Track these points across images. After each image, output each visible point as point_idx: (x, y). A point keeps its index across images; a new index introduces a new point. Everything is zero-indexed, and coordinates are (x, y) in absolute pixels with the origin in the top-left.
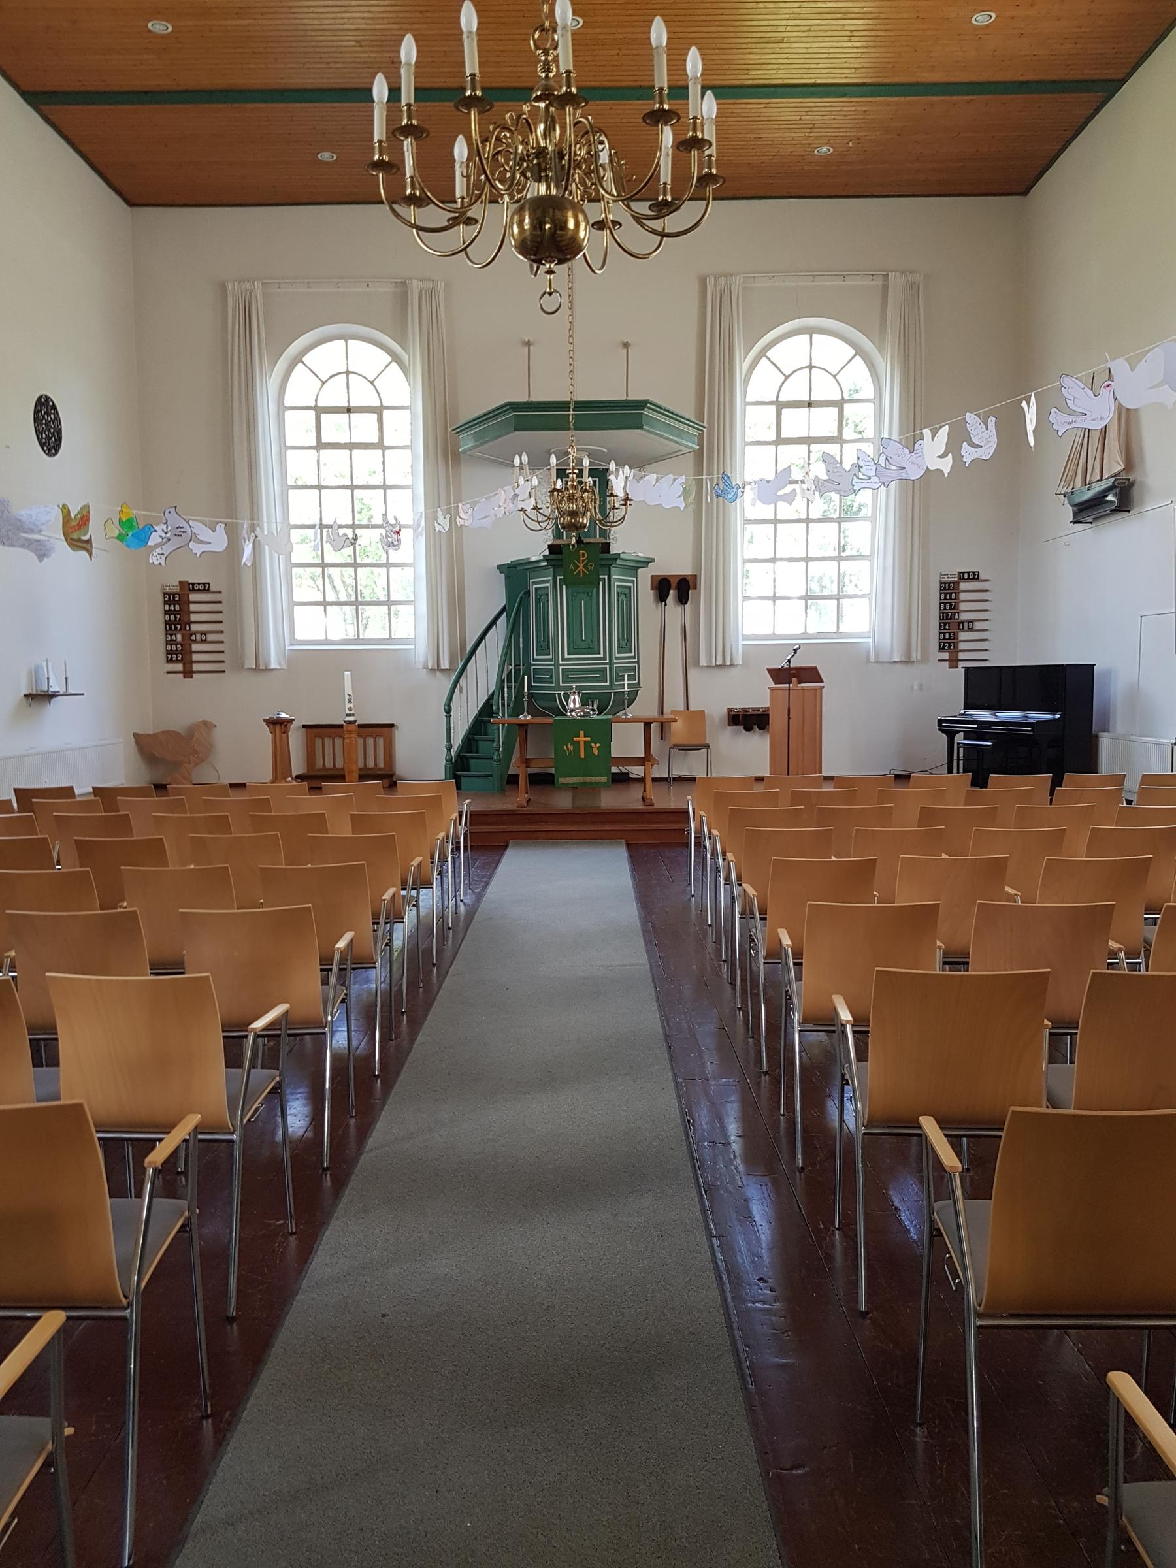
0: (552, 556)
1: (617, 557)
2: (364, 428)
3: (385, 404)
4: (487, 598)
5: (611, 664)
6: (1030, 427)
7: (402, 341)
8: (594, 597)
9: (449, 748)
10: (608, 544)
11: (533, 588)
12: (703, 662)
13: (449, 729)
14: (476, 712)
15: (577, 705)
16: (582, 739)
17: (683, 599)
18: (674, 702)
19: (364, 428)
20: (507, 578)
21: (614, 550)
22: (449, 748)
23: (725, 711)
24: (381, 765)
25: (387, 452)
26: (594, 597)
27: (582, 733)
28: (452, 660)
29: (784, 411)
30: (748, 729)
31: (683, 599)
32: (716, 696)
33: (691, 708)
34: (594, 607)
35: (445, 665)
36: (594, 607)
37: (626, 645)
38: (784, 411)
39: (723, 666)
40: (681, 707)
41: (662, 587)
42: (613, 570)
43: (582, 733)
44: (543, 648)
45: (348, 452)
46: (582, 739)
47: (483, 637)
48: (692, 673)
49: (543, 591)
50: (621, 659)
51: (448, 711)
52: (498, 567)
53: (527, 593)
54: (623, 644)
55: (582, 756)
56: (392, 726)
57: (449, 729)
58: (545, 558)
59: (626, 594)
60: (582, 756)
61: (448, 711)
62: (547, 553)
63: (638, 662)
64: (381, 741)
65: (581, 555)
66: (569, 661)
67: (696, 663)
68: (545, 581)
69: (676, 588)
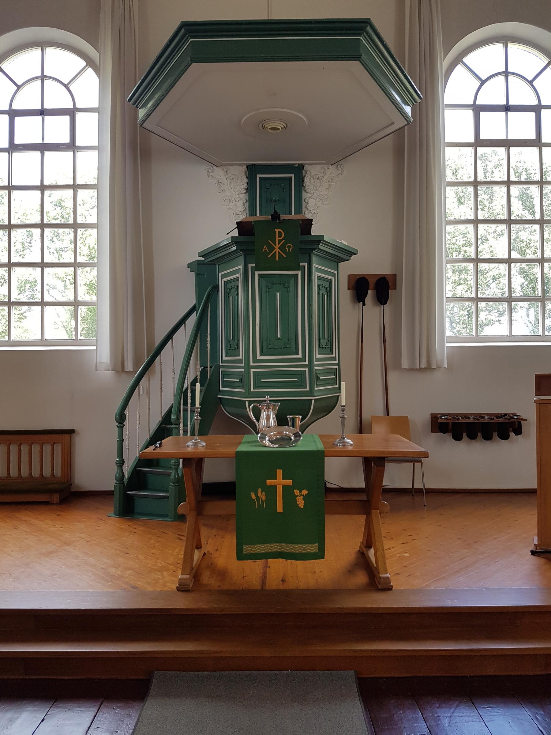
0: (243, 239)
1: (319, 240)
2: (57, 130)
3: (78, 106)
4: (178, 296)
5: (310, 366)
6: (182, 400)
7: (93, 40)
8: (292, 293)
9: (121, 463)
10: (309, 222)
11: (221, 282)
12: (405, 364)
13: (121, 442)
14: (160, 419)
15: (272, 423)
16: (280, 481)
17: (382, 299)
18: (373, 406)
19: (57, 130)
20: (198, 275)
21: (315, 231)
22: (121, 463)
23: (429, 417)
24: (58, 472)
25: (79, 154)
26: (292, 288)
27: (279, 472)
28: (136, 365)
29: (482, 114)
30: (457, 437)
31: (382, 299)
32: (418, 400)
33: (392, 414)
34: (292, 302)
35: (129, 367)
36: (292, 302)
37: (327, 345)
38: (482, 114)
39: (421, 370)
40: (380, 411)
41: (360, 287)
42: (314, 259)
43: (279, 472)
44: (232, 348)
45: (38, 154)
46: (280, 481)
47: (169, 336)
48: (392, 377)
49: (232, 284)
50: (322, 362)
51: (121, 419)
52: (189, 265)
53: (216, 288)
54: (324, 343)
55: (280, 509)
56: (72, 432)
57: (121, 442)
58: (234, 241)
59: (327, 288)
60: (280, 509)
61: (121, 419)
62: (236, 233)
63: (339, 364)
64: (58, 448)
65: (275, 236)
66: (262, 362)
67: (398, 366)
68: (233, 272)
69: (375, 289)
